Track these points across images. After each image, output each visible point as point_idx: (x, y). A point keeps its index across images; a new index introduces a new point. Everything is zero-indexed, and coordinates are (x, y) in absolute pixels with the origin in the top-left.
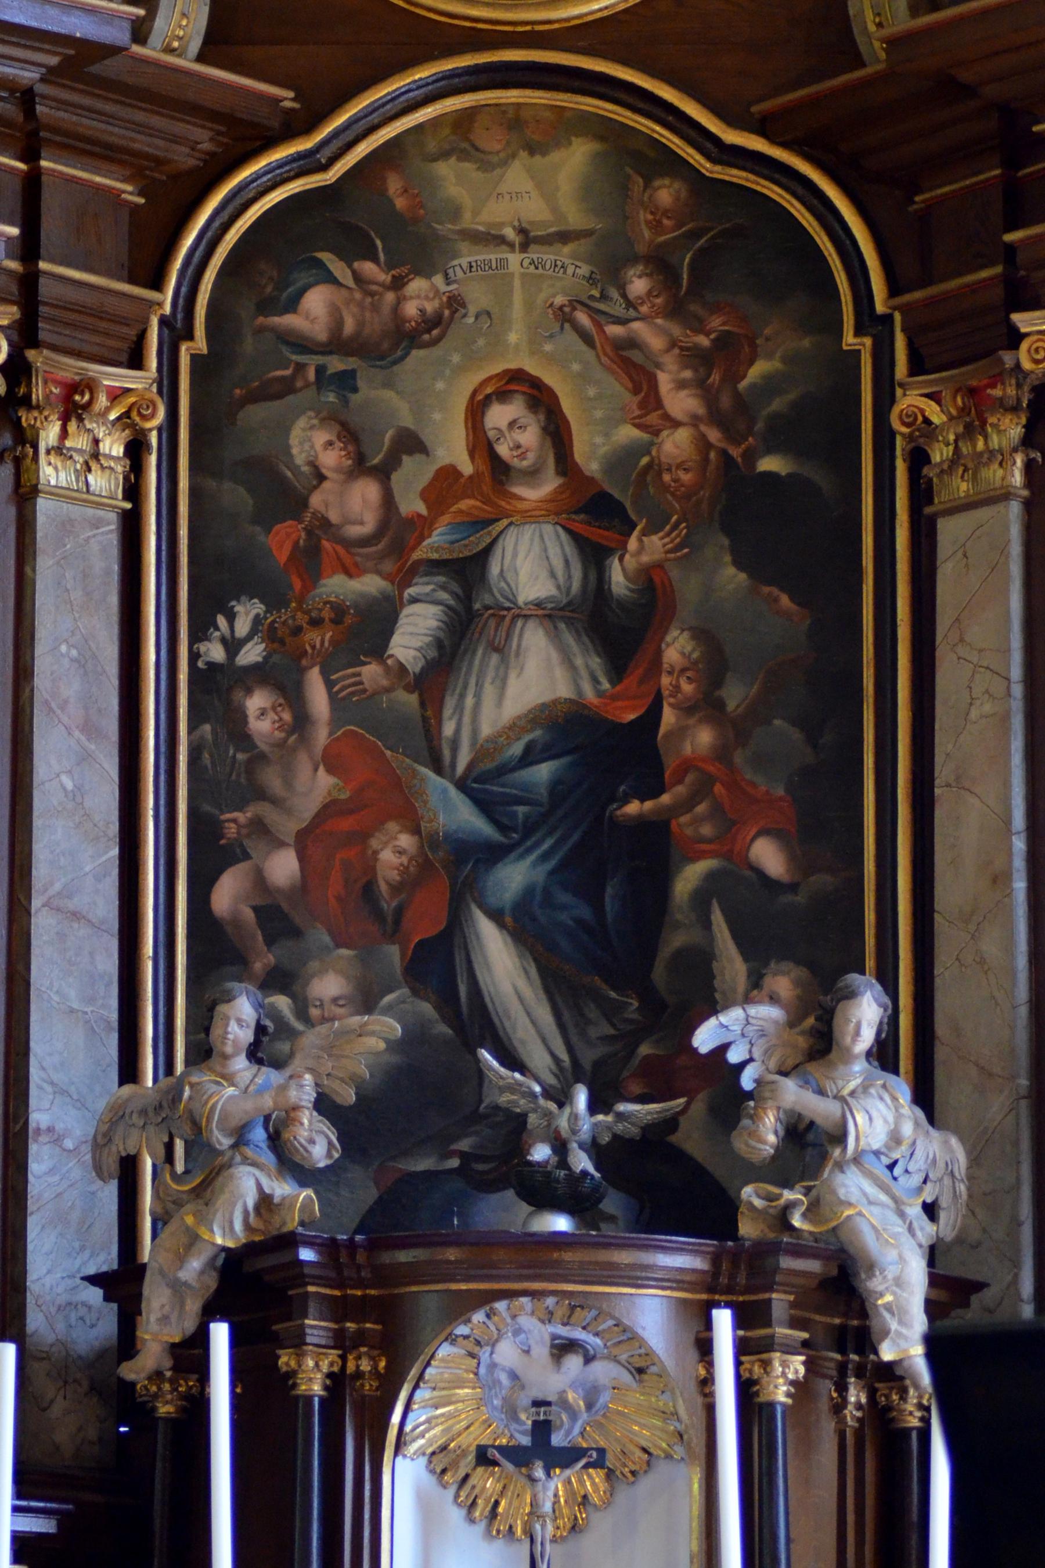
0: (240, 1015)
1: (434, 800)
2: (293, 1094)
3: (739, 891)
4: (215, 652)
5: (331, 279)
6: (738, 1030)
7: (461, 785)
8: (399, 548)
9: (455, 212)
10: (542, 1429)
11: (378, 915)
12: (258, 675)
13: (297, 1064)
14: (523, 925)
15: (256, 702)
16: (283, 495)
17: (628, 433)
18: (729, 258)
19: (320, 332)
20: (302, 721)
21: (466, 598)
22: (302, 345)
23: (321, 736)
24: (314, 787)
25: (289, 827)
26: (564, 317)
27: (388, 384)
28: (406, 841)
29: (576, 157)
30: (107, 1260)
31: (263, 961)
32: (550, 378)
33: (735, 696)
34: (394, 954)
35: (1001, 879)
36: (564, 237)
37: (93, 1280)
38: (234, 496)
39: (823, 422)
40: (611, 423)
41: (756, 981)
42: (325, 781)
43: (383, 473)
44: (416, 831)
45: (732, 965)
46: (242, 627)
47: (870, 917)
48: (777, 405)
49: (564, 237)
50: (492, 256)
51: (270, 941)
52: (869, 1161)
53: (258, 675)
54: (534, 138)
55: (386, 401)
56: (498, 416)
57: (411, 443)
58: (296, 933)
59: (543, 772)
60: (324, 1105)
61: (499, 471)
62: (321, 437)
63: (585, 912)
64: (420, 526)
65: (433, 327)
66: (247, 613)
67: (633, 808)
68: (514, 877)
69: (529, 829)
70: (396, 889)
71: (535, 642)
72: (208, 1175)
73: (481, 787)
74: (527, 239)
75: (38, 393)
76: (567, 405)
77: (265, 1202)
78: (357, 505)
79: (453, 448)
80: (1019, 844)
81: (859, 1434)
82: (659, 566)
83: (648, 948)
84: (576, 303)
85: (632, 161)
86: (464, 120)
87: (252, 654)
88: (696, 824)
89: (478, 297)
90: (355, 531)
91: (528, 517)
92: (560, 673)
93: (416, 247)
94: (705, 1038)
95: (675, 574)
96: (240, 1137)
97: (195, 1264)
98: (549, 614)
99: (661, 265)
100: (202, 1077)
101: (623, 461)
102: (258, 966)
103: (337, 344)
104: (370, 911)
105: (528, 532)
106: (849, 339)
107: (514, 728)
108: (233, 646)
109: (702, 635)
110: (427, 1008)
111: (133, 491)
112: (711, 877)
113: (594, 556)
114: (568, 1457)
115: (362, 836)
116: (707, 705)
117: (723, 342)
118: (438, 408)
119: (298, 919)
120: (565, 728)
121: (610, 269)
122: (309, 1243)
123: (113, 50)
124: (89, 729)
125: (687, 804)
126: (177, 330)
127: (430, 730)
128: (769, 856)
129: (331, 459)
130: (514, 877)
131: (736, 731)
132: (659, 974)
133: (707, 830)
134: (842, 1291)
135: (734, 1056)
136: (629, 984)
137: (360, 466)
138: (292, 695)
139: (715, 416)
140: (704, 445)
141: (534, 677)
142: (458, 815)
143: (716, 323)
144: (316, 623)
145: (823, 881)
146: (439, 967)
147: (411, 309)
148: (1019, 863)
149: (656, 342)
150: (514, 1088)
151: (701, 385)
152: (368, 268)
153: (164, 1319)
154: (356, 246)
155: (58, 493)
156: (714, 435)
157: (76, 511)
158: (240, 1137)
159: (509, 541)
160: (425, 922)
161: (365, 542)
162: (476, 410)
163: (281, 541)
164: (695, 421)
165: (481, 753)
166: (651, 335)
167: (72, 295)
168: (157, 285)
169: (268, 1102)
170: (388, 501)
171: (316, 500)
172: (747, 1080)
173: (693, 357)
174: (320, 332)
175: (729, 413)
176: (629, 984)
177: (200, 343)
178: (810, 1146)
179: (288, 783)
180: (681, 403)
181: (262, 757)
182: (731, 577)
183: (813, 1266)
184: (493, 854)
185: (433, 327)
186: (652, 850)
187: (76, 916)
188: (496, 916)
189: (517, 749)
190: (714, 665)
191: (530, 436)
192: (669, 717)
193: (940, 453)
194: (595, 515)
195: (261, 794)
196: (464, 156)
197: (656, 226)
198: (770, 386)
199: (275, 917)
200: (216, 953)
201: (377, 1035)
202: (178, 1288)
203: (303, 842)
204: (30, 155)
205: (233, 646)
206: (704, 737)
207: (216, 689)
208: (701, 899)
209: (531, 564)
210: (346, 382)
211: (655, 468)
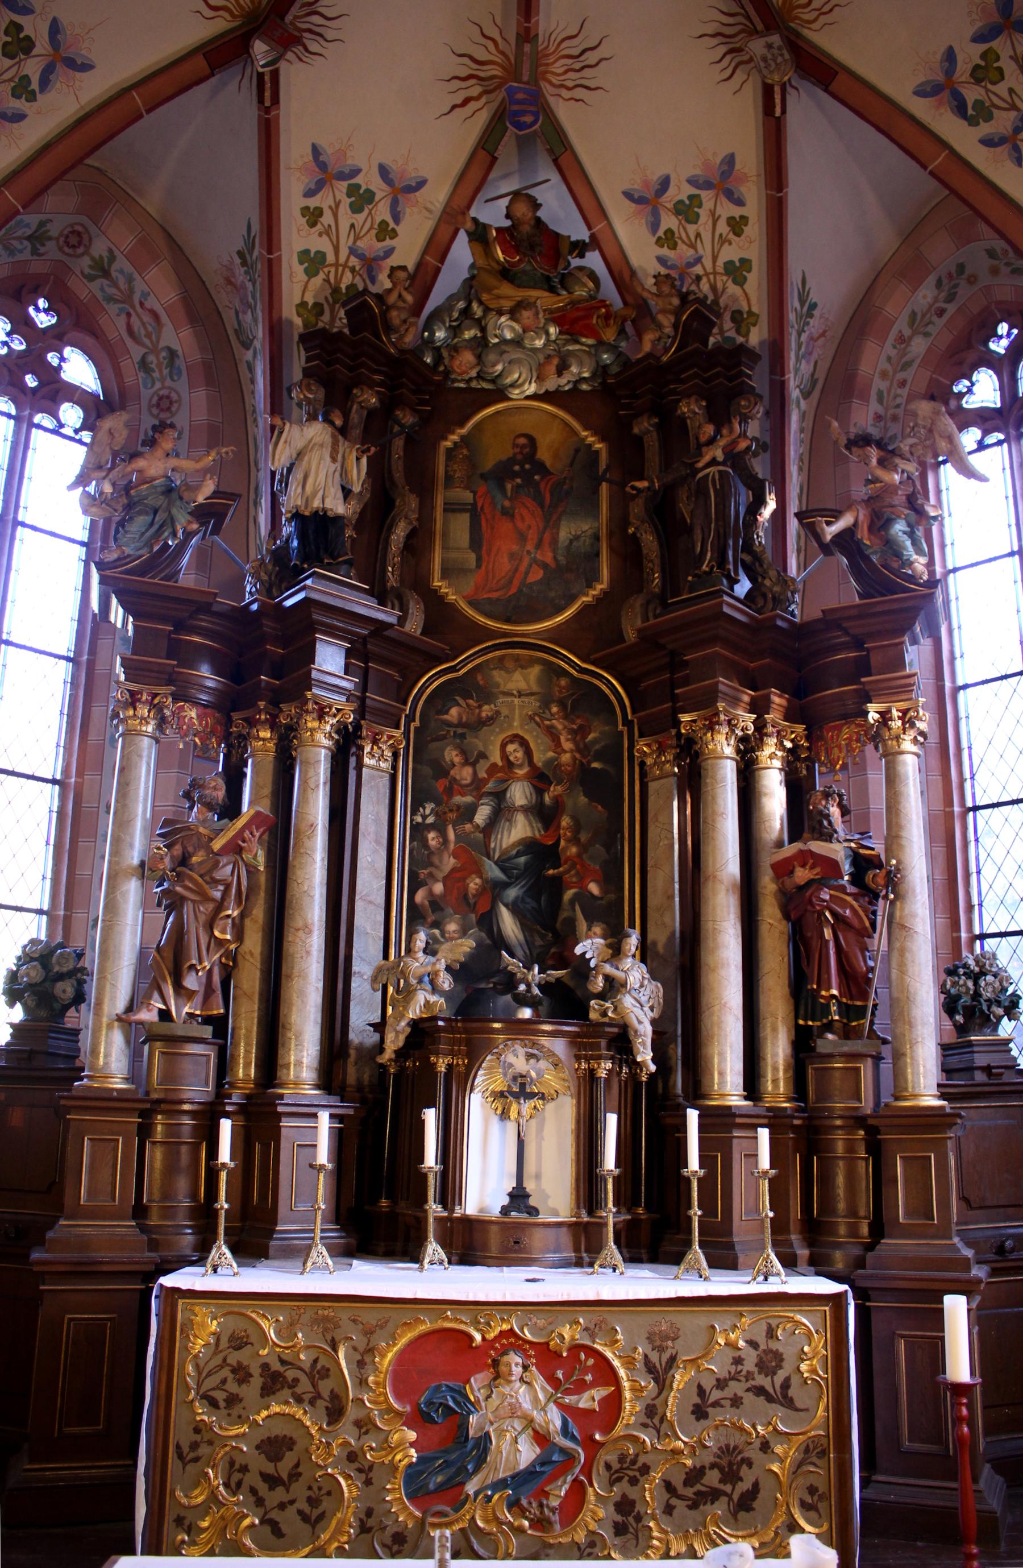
0: (421, 939)
1: (487, 868)
2: (438, 966)
3: (584, 899)
4: (419, 819)
5: (459, 705)
6: (590, 946)
7: (496, 863)
8: (478, 788)
9: (498, 685)
10: (523, 1085)
11: (468, 904)
12: (432, 827)
13: (439, 956)
14: (515, 909)
15: (431, 835)
16: (442, 770)
17: (550, 754)
18: (583, 701)
19: (455, 720)
20: (445, 841)
21: (499, 805)
22: (449, 724)
23: (452, 846)
24: (450, 862)
25: (441, 875)
26: (531, 718)
27: (476, 737)
28: (478, 881)
29: (535, 670)
30: (376, 1018)
31: (431, 918)
32: (527, 737)
33: (584, 837)
34: (473, 917)
35: (671, 897)
36: (532, 694)
37: (370, 1025)
38: (427, 770)
39: (612, 753)
40: (545, 751)
41: (589, 929)
42: (452, 861)
43: (474, 765)
44: (481, 877)
45: (582, 925)
46: (428, 812)
47: (626, 908)
48: (597, 747)
49: (532, 694)
50: (510, 699)
51: (433, 912)
52: (633, 992)
53: (432, 827)
54: (523, 664)
55: (476, 743)
56: (510, 748)
57: (483, 756)
58: (442, 910)
59: (522, 860)
60: (448, 969)
61: (510, 765)
62: (454, 753)
63: (534, 904)
64: (485, 781)
65: (491, 720)
66: (429, 807)
67: (551, 872)
68: (512, 893)
69: (517, 878)
70: (474, 896)
71: (520, 819)
72: (407, 994)
73: (503, 864)
74: (520, 694)
75: (364, 733)
76: (532, 745)
77: (427, 1002)
78: (465, 774)
79: (496, 758)
80: (677, 886)
81: (626, 1082)
82: (560, 796)
83: (555, 916)
84: (535, 714)
85: (553, 672)
86: (501, 659)
87: (430, 820)
88: (571, 877)
89: (505, 712)
90: (464, 782)
91: (519, 779)
92: (528, 829)
93: (486, 695)
94: (578, 950)
95: (565, 798)
96: (420, 981)
97: (403, 1024)
98: (526, 810)
99: (562, 704)
100: (408, 960)
101: (549, 763)
102: (429, 920)
103: (460, 724)
104: (465, 903)
105: (519, 784)
106: (620, 727)
107: (514, 846)
108: (424, 817)
109: (573, 817)
110: (483, 935)
111: (394, 767)
112: (575, 894)
113: (540, 792)
114: (532, 1095)
115: (465, 879)
116: (575, 840)
117: (581, 727)
118: (493, 747)
119: (442, 905)
120: (528, 846)
121: (546, 704)
122: (442, 1019)
123: (390, 626)
124: (377, 842)
125: (568, 871)
126: (410, 718)
127: (487, 845)
128: (594, 888)
129: (457, 760)
130: (512, 893)
131: (584, 848)
132: (558, 925)
133: (574, 880)
134: (622, 1042)
135: (588, 956)
136: (552, 942)
137: (466, 762)
138: (443, 834)
139: (578, 750)
140: (574, 759)
141: (519, 830)
142: (495, 873)
143: (579, 721)
144: (451, 811)
145: (612, 896)
146: (488, 922)
147: (484, 714)
148: (677, 892)
149: (560, 727)
150: (513, 964)
151: (573, 740)
152: (471, 702)
153: (392, 1042)
154: (467, 696)
155: (369, 767)
156: (578, 756)
157: (376, 773)
158: (420, 981)
159: (513, 787)
160: (483, 907)
161: (467, 786)
162: (503, 746)
163: (440, 785)
164: (572, 751)
165: (503, 853)
166: (558, 725)
167: (377, 705)
168: (405, 703)
169: (429, 969)
170: (475, 773)
171: (452, 772)
172: (592, 964)
173: (572, 731)
174: (455, 720)
175: (582, 749)
176: (552, 942)
177: (417, 723)
178: (613, 987)
179: (441, 862)
180: (567, 745)
181: (431, 853)
182: (583, 800)
183: (615, 1030)
184: (506, 885)
185: (491, 720)
186: (557, 885)
187: (370, 902)
188: (506, 905)
189: (514, 852)
190: (577, 827)
191: (520, 754)
192: (562, 843)
193: (649, 761)
194: (540, 779)
195: (432, 865)
196: (501, 669)
197: (560, 692)
198: (595, 741)
199: (435, 904)
200: (416, 916)
201: (467, 945)
202: (397, 1032)
203: (445, 880)
204: (366, 663)
205: (424, 817)
206: (574, 850)
207: (418, 831)
208: (572, 902)
209: (519, 794)
210: (463, 736)
211: (559, 765)
